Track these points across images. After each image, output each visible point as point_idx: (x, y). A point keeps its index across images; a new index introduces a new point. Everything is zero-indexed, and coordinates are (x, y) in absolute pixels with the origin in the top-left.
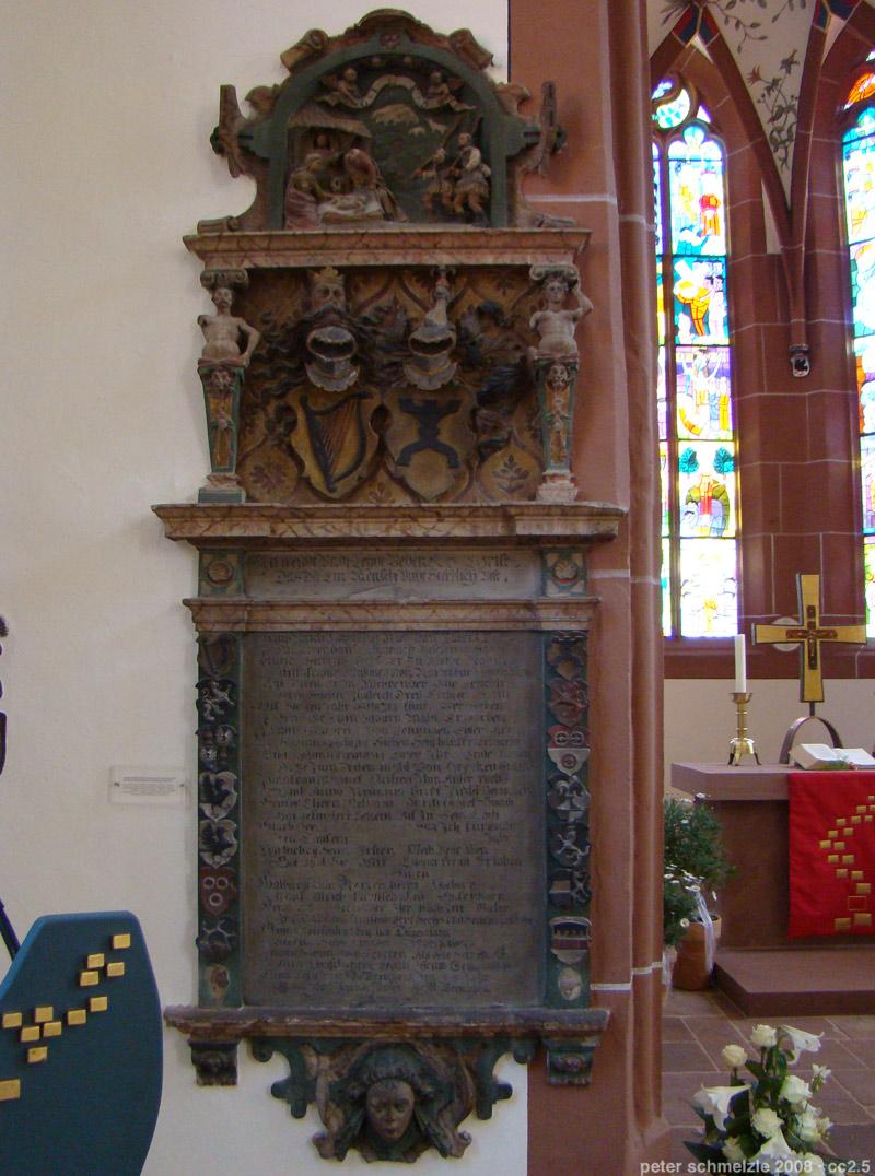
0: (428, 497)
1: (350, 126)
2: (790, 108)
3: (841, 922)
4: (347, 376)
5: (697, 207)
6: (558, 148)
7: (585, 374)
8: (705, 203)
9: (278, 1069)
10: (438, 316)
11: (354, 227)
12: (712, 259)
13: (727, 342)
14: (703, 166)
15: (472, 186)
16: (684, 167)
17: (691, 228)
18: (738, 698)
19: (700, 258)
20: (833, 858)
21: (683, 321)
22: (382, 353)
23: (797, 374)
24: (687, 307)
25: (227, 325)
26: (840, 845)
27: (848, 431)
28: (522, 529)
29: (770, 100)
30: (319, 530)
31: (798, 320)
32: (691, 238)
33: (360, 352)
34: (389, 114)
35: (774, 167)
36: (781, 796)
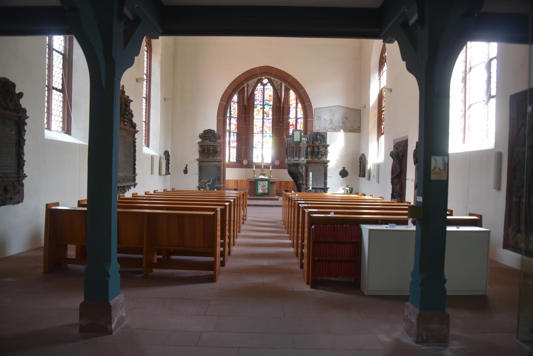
0: (211, 159)
6: (219, 138)
7: (220, 152)
8: (270, 96)
11: (207, 142)
12: (270, 105)
19: (268, 105)
21: (265, 115)
24: (266, 113)
32: (267, 102)
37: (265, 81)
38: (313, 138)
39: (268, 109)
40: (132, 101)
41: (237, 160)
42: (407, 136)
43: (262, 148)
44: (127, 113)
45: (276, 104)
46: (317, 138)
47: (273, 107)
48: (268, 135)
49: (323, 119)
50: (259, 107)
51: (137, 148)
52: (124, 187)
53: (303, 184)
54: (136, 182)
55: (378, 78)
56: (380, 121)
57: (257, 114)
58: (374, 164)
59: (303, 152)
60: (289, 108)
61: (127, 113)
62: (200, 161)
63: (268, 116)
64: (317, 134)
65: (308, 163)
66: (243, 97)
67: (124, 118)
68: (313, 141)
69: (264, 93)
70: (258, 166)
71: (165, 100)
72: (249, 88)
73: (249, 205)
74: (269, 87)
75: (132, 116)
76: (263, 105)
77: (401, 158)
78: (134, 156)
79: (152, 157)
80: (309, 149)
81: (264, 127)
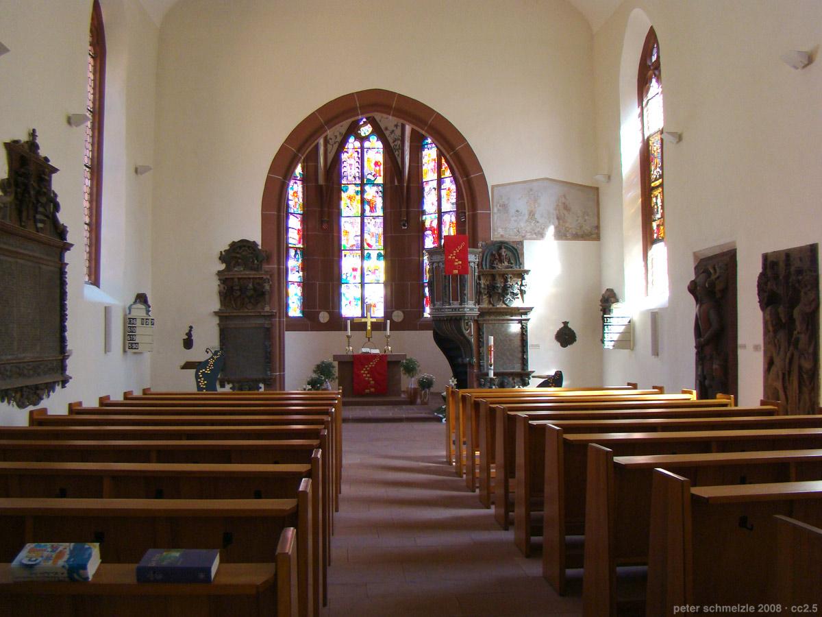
1: (238, 255)
2: (398, 139)
3: (367, 391)
4: (239, 293)
5: (373, 166)
6: (268, 259)
7: (271, 292)
8: (376, 164)
9: (231, 385)
10: (251, 285)
11: (239, 271)
12: (378, 185)
13: (382, 215)
14: (376, 150)
15: (256, 266)
16: (369, 151)
17: (371, 174)
18: (348, 337)
19: (374, 185)
20: (365, 375)
21: (367, 208)
22: (243, 290)
23: (403, 228)
24: (369, 203)
25: (222, 286)
26: (366, 372)
27: (419, 247)
28: (262, 314)
29: (392, 136)
30: (235, 314)
31: (404, 209)
33: (240, 290)
34: (244, 253)
35: (395, 157)
36: (352, 360)
37: (366, 130)
38: (492, 255)
39: (371, 193)
40: (55, 170)
41: (303, 312)
42: (734, 242)
43: (363, 284)
44: (43, 200)
45: (392, 182)
46: (500, 255)
47: (384, 188)
48: (374, 254)
49: (512, 211)
50: (352, 190)
51: (69, 289)
52: (37, 387)
53: (471, 365)
54: (68, 373)
55: (639, 110)
56: (647, 212)
57: (349, 206)
58: (644, 313)
59: (470, 289)
60: (422, 189)
61: (43, 200)
62: (222, 316)
63: (373, 209)
64: (501, 245)
65: (483, 313)
66: (316, 168)
67: (36, 212)
68: (492, 263)
69: (364, 158)
70: (359, 326)
71: (136, 171)
72: (329, 147)
73: (345, 420)
74: (375, 144)
75: (57, 207)
76: (362, 185)
77: (718, 295)
78: (63, 307)
79: (107, 310)
80: (482, 282)
81: (366, 236)
